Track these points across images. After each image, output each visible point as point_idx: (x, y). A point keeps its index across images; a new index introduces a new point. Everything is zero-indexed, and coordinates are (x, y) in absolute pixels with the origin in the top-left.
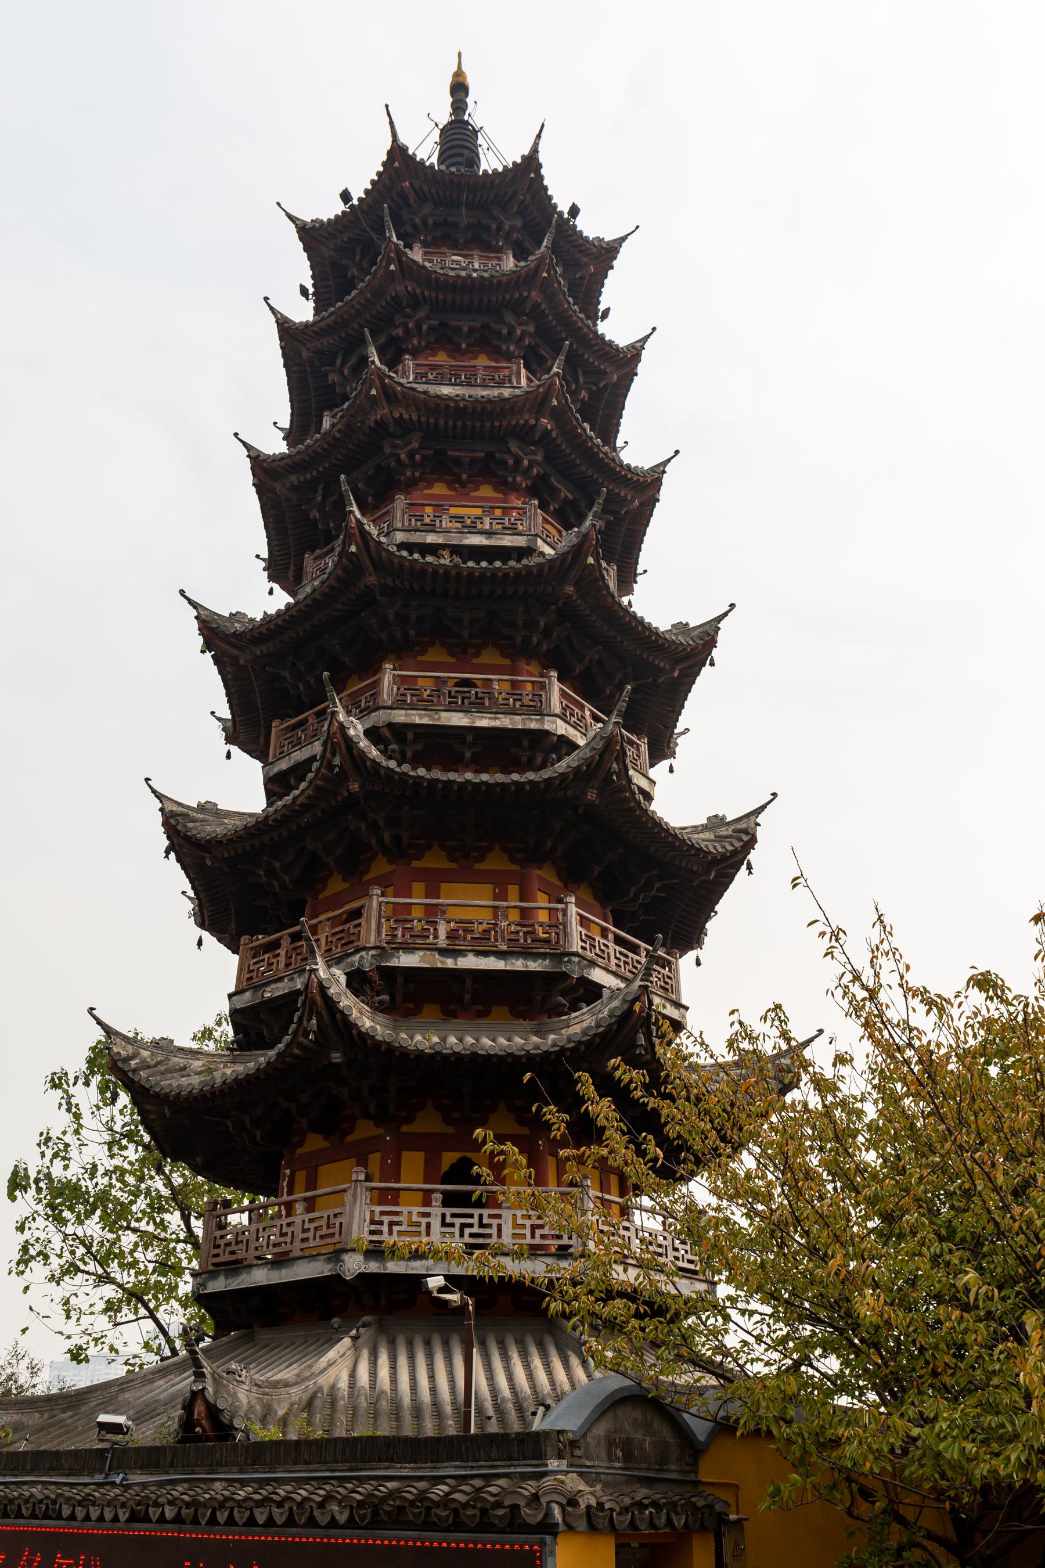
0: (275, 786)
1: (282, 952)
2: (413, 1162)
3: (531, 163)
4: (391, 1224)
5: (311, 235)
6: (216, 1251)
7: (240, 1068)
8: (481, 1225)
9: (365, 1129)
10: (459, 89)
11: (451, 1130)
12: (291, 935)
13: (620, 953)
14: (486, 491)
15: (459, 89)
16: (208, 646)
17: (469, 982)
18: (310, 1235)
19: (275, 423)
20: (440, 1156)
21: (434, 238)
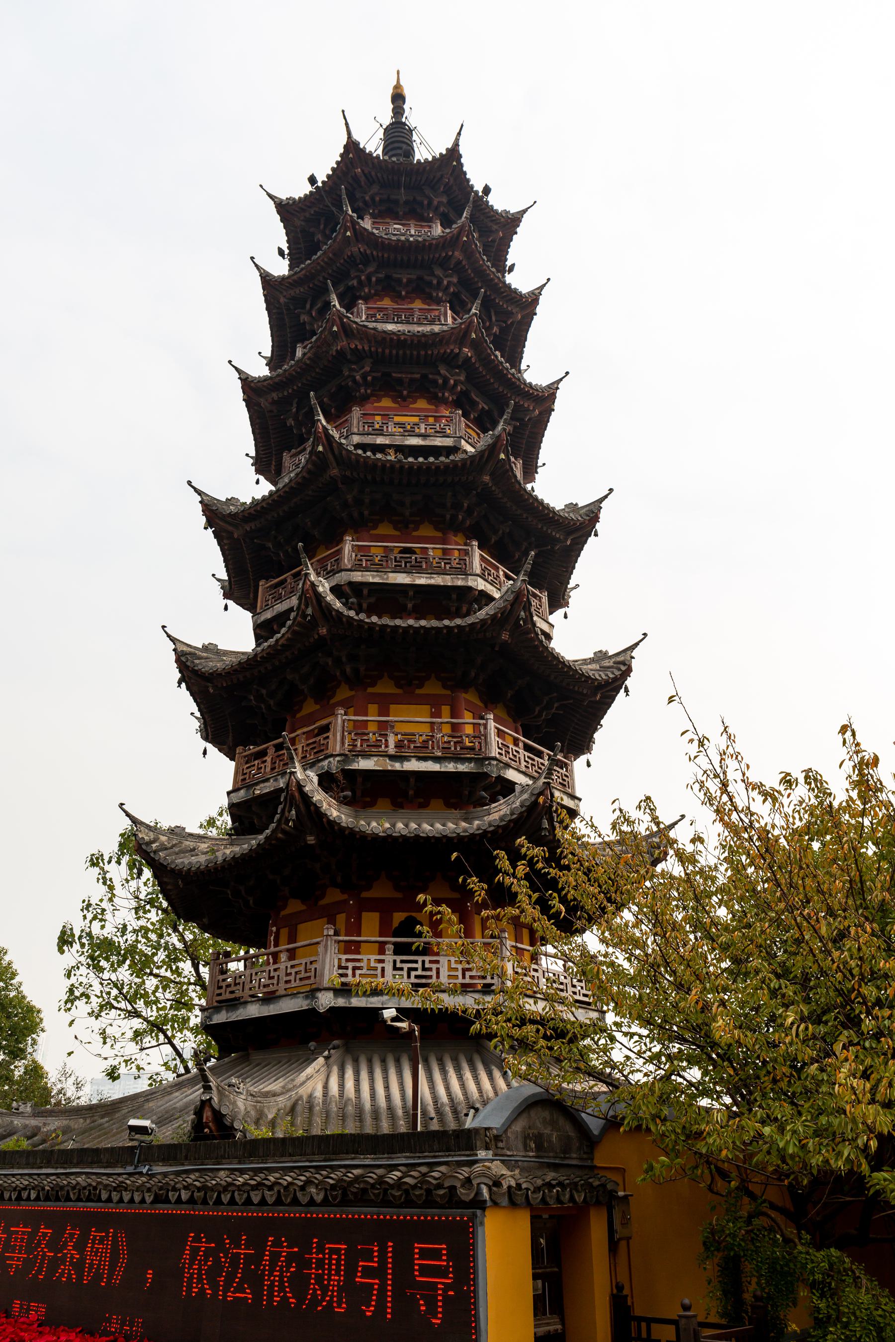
2: (371, 920)
3: (453, 154)
4: (354, 969)
5: (287, 210)
6: (219, 991)
7: (237, 849)
8: (424, 969)
9: (333, 896)
10: (398, 98)
12: (275, 746)
13: (529, 757)
14: (422, 404)
15: (398, 98)
16: (210, 524)
17: (412, 780)
18: (292, 978)
19: (260, 353)
21: (380, 212)
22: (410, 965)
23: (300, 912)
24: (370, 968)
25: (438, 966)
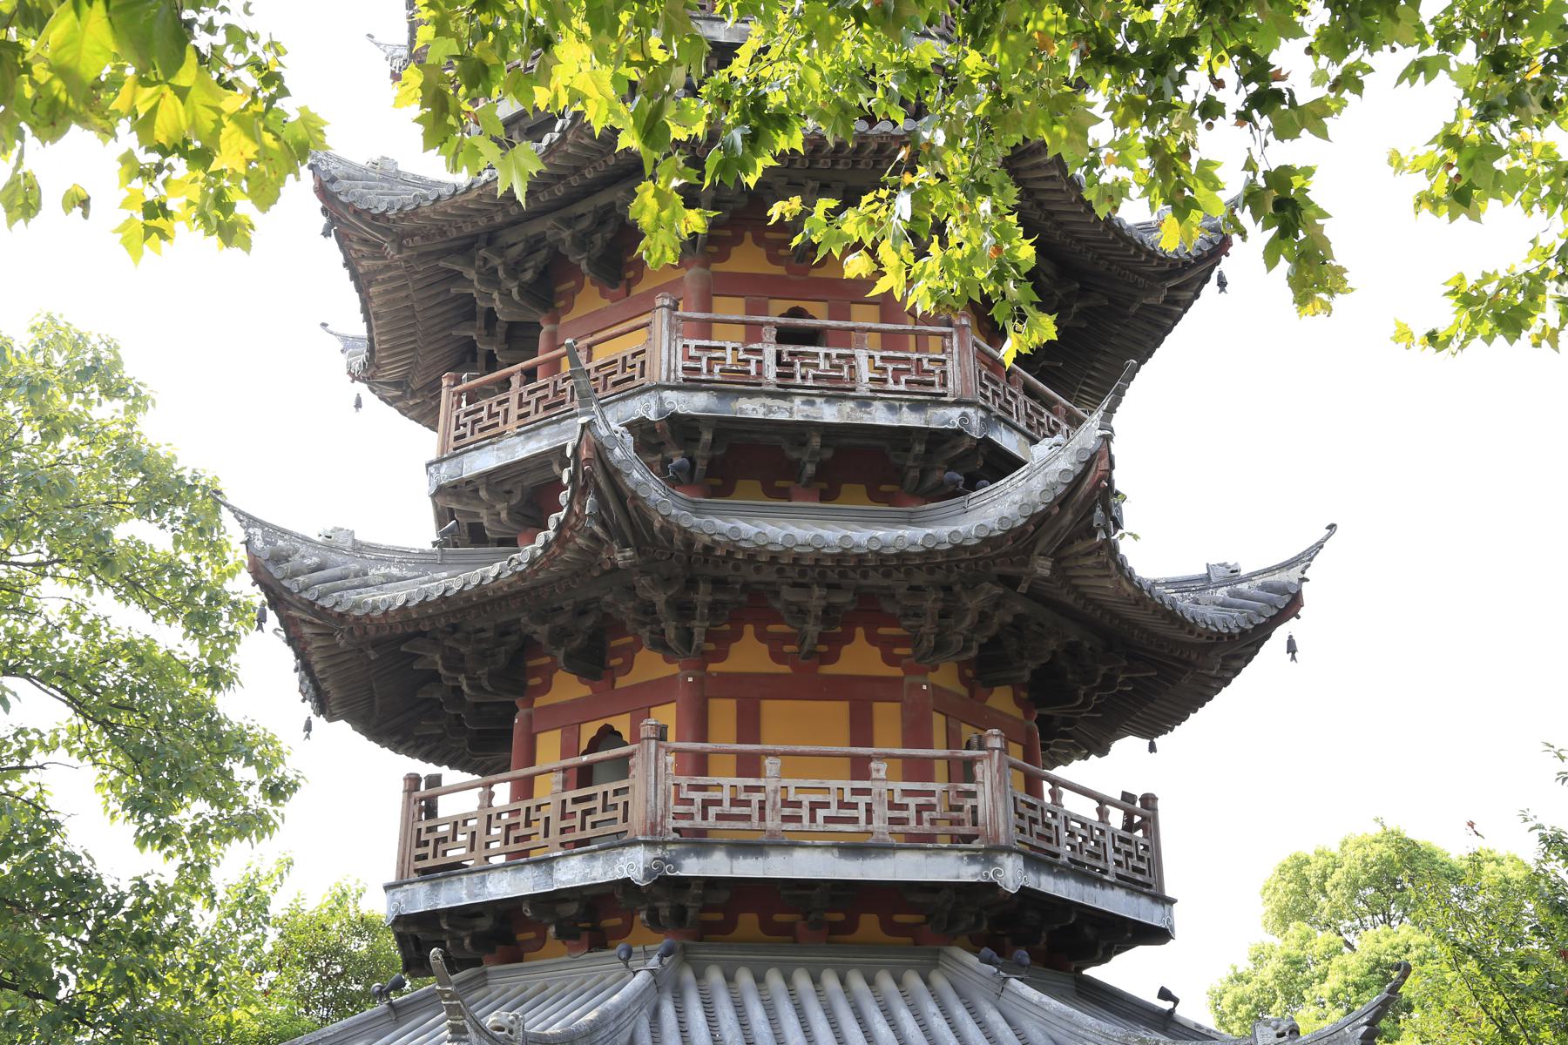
0: (468, 513)
1: (513, 395)
4: (920, 809)
6: (420, 851)
7: (474, 576)
8: (842, 805)
9: (650, 666)
11: (785, 669)
20: (870, 709)
22: (922, 800)
23: (575, 702)
24: (842, 805)
25: (867, 799)
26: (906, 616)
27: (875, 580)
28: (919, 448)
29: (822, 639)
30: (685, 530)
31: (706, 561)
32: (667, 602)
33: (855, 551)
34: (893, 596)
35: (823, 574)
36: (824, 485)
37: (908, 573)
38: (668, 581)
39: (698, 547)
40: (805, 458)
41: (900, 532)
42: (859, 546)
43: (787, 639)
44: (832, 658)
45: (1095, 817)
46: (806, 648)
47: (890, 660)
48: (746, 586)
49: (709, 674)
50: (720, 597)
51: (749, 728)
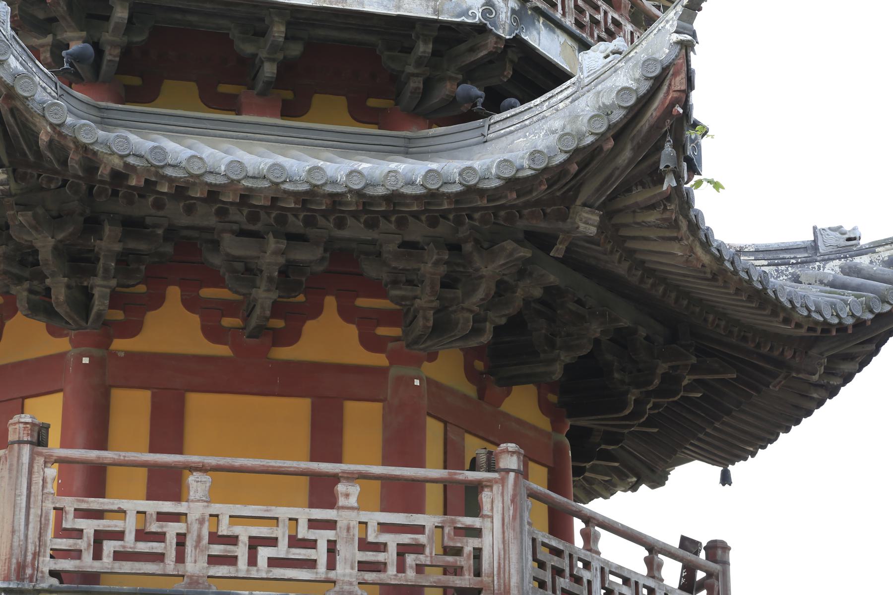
8: (295, 542)
11: (223, 350)
20: (341, 409)
22: (406, 538)
24: (295, 542)
25: (330, 534)
26: (395, 283)
27: (355, 230)
28: (424, 48)
29: (277, 309)
30: (85, 148)
31: (115, 193)
32: (55, 248)
33: (329, 189)
34: (379, 254)
35: (281, 220)
36: (289, 95)
37: (402, 223)
38: (58, 219)
39: (104, 172)
40: (263, 54)
41: (393, 166)
42: (334, 182)
43: (228, 309)
44: (291, 336)
45: (643, 570)
46: (254, 322)
47: (370, 343)
48: (171, 232)
49: (114, 354)
50: (132, 245)
51: (168, 431)
